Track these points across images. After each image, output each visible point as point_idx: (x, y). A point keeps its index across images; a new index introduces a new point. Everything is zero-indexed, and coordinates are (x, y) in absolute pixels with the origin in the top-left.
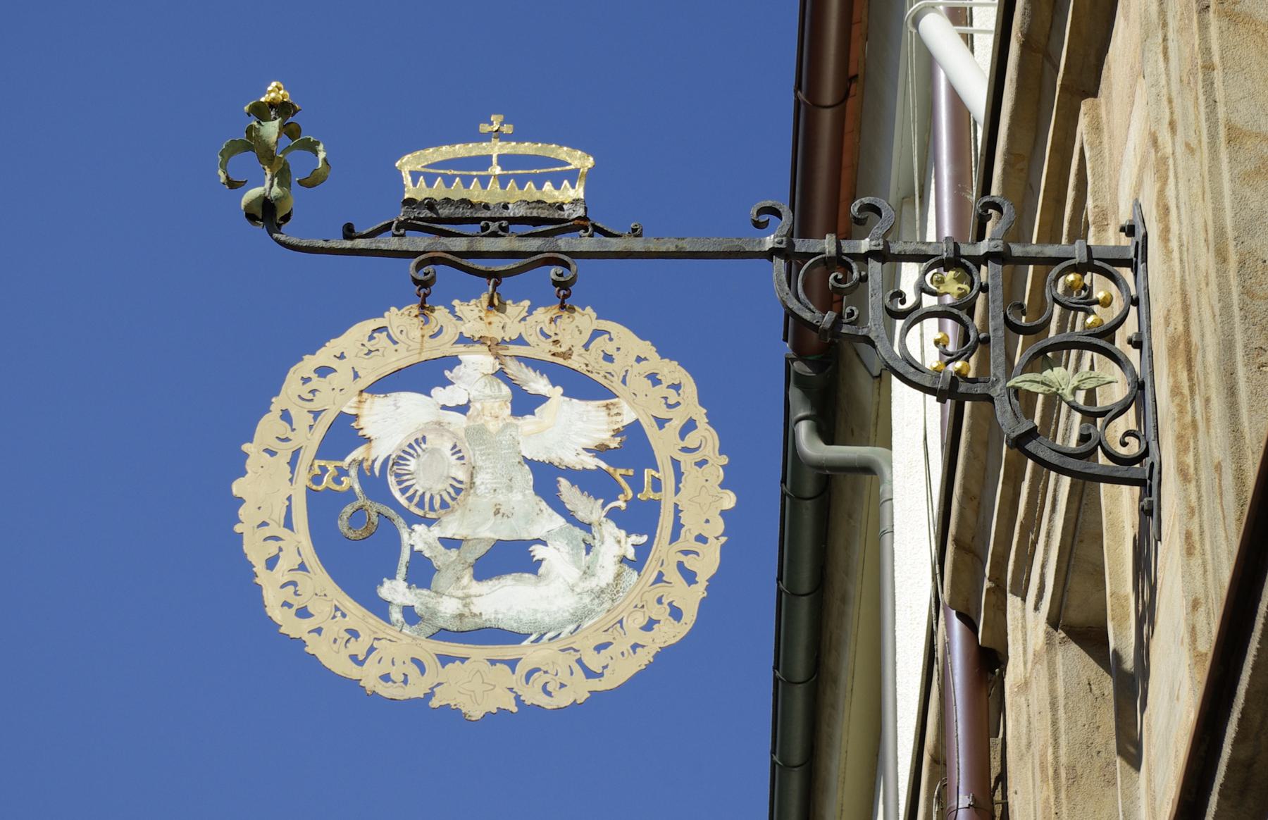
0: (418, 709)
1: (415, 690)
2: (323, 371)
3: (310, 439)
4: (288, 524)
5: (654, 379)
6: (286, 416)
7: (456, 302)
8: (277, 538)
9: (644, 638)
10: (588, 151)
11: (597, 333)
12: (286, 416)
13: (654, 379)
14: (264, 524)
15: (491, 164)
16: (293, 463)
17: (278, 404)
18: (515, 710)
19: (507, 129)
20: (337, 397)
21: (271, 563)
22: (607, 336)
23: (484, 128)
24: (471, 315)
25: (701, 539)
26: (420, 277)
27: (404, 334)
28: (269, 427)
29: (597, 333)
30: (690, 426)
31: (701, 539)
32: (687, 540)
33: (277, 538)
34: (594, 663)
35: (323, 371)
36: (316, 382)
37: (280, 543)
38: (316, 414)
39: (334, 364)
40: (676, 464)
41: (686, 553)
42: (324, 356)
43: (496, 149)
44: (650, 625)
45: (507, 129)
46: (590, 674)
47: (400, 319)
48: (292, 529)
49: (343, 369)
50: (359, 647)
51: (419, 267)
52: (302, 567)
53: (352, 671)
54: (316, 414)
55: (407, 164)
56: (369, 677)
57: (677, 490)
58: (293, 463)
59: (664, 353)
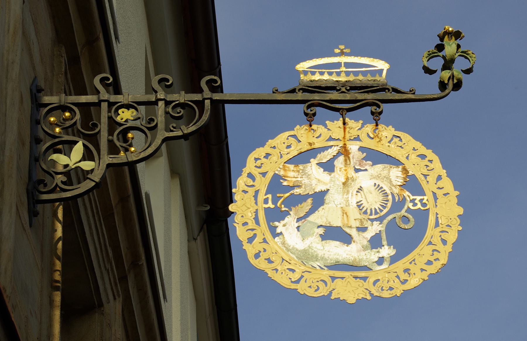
0: (326, 300)
1: (323, 291)
2: (429, 263)
3: (262, 184)
4: (257, 222)
5: (270, 261)
6: (444, 242)
7: (369, 297)
8: (439, 188)
9: (270, 151)
10: (387, 61)
11: (297, 282)
12: (444, 242)
13: (270, 261)
14: (445, 195)
15: (341, 66)
16: (256, 197)
17: (449, 248)
18: (327, 122)
19: (347, 51)
20: (273, 167)
21: (439, 178)
22: (293, 280)
23: (337, 51)
24: (335, 127)
25: (245, 192)
26: (309, 111)
27: (305, 136)
28: (452, 237)
29: (297, 282)
30: (251, 240)
31: (245, 192)
32: (251, 191)
33: (439, 188)
34: (292, 139)
35: (429, 263)
36: (432, 259)
37: (254, 232)
38: (430, 243)
39: (425, 267)
40: (257, 222)
41: (253, 186)
42: (266, 149)
43: (344, 59)
44: (267, 156)
45: (347, 51)
46: (294, 136)
47: (301, 131)
48: (260, 226)
49: (275, 153)
50: (295, 277)
51: (308, 107)
52: (425, 176)
53: (293, 286)
54: (430, 243)
55: (303, 66)
56: (302, 288)
57: (256, 212)
58: (256, 197)
59: (263, 273)
